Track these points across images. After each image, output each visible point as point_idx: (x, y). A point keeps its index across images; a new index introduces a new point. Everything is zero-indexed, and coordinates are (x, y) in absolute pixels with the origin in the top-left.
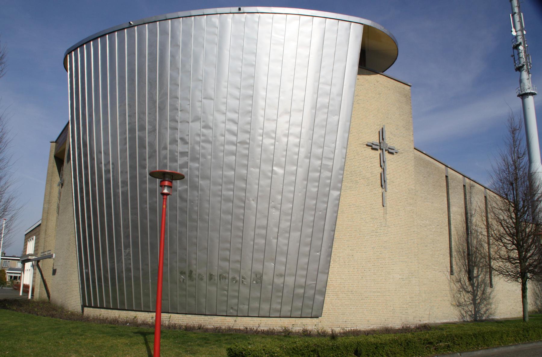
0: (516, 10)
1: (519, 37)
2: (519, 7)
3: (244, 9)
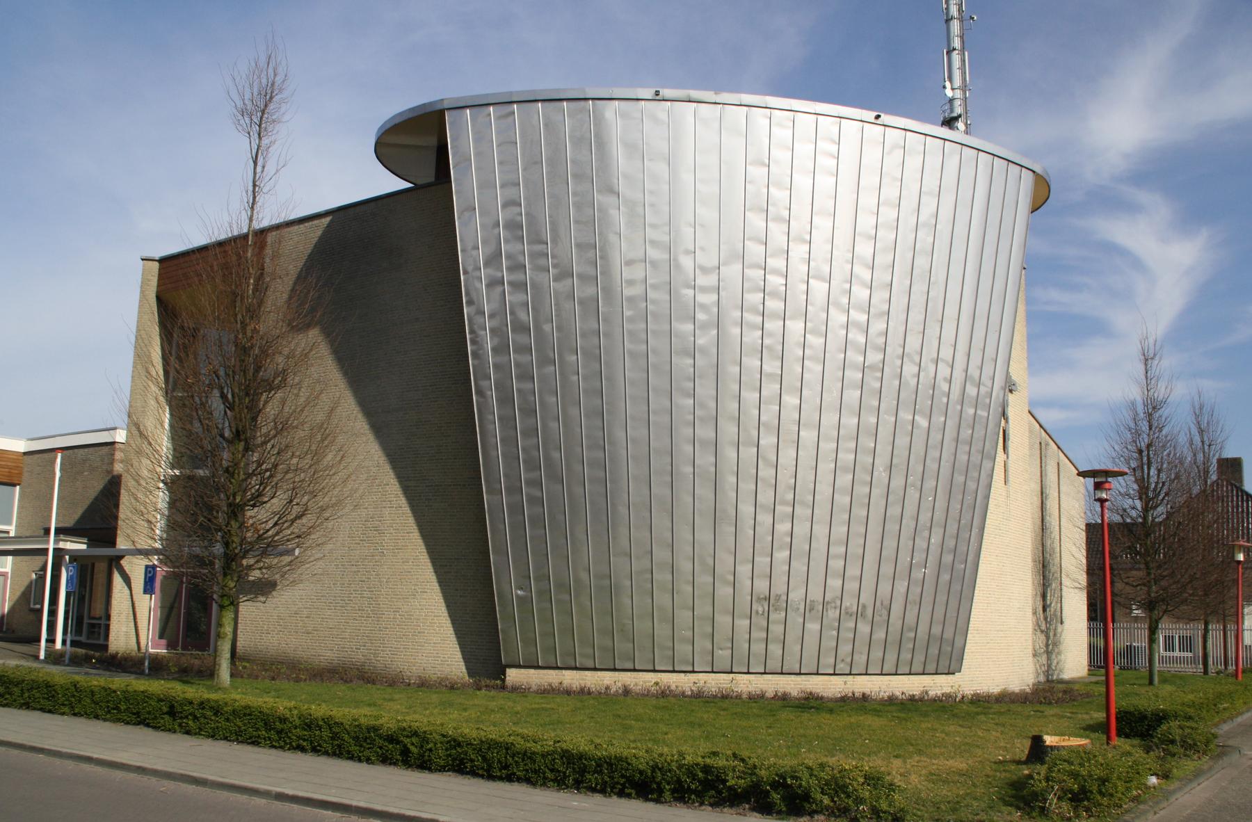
0: (957, 43)
1: (957, 103)
2: (962, 37)
3: (885, 118)
